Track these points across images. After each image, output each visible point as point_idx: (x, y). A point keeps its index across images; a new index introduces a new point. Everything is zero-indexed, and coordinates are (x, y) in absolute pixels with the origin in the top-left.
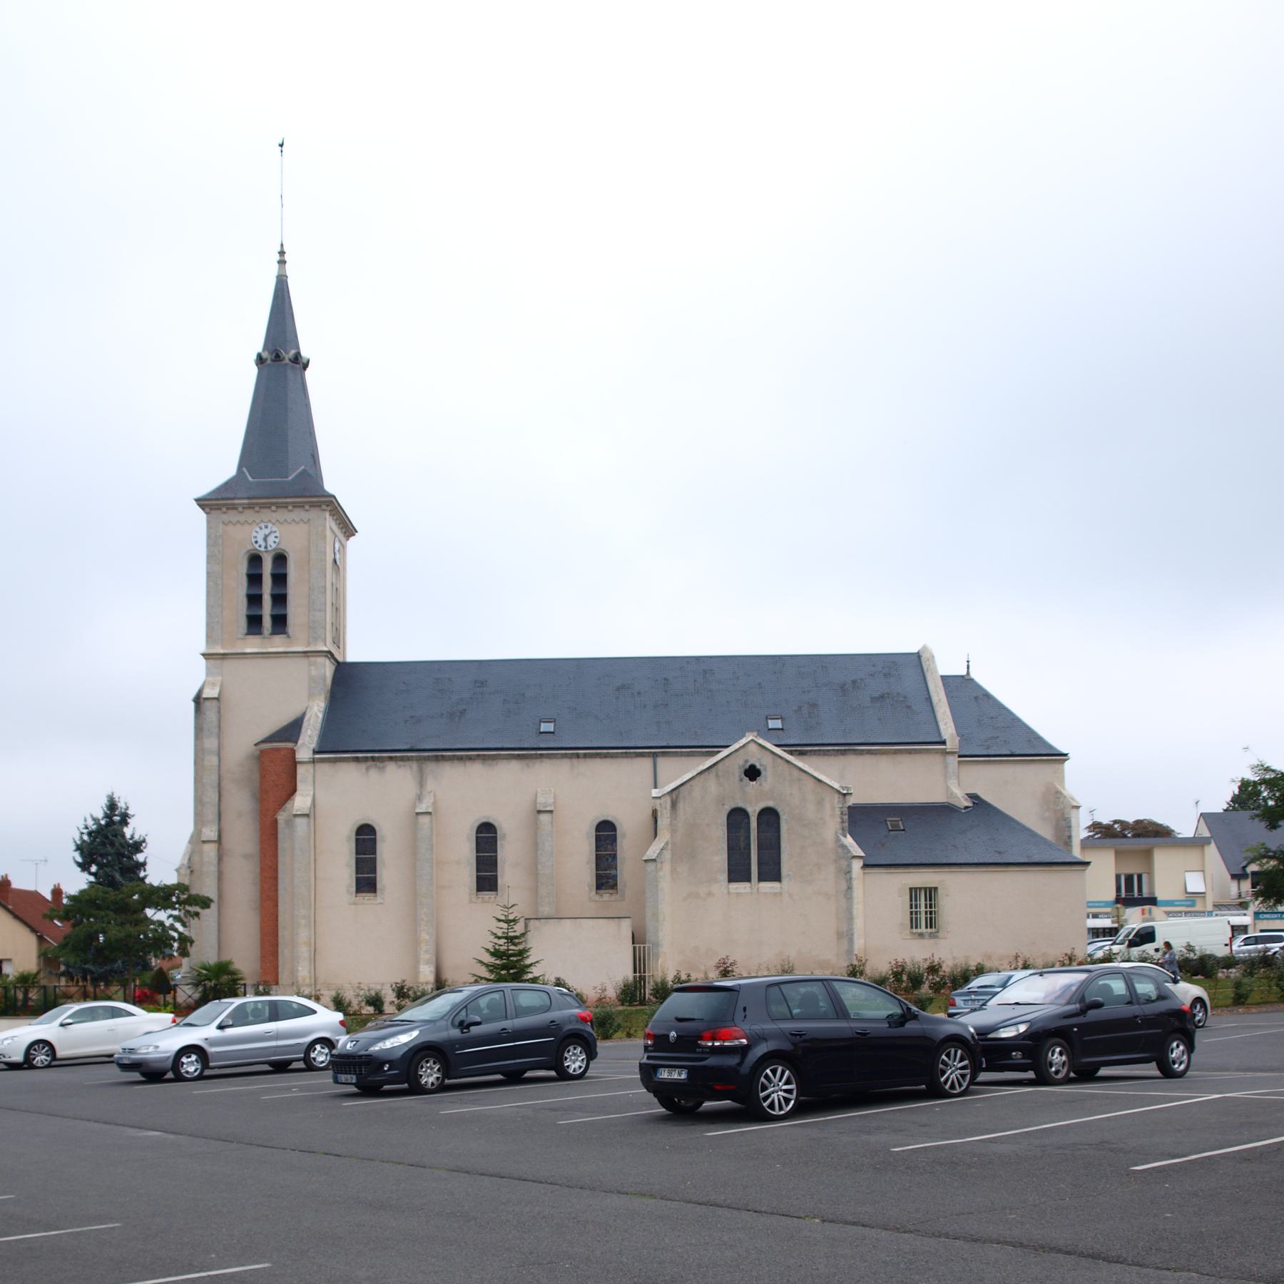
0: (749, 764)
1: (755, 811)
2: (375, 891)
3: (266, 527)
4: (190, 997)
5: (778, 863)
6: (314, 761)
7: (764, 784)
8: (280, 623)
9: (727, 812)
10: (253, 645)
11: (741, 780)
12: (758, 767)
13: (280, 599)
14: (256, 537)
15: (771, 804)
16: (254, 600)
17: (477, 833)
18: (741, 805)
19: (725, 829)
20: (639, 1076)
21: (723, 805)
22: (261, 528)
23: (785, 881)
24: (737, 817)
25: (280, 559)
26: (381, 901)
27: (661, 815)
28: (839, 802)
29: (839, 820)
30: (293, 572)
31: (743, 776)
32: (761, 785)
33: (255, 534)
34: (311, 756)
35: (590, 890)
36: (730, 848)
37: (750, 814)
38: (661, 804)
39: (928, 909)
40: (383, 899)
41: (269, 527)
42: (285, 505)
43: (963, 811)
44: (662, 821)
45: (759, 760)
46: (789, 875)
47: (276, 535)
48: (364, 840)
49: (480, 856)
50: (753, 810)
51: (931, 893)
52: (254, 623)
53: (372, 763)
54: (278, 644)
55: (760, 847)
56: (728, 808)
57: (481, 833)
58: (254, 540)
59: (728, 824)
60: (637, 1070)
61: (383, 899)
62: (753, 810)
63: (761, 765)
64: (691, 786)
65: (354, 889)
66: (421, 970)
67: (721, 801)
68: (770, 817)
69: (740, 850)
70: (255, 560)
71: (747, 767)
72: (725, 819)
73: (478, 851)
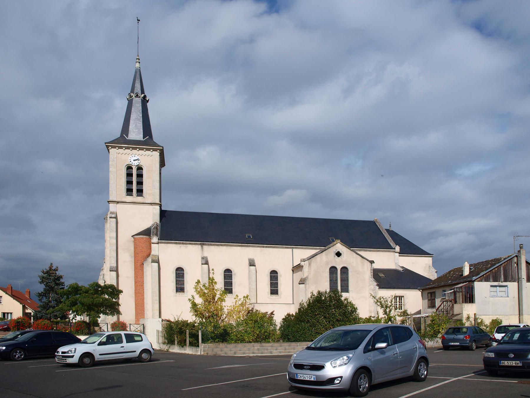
0: (337, 251)
1: (340, 267)
2: (184, 292)
3: (135, 156)
4: (137, 329)
5: (348, 286)
6: (158, 243)
7: (343, 258)
8: (140, 192)
9: (330, 267)
10: (129, 199)
11: (335, 257)
12: (341, 252)
13: (140, 183)
14: (131, 161)
15: (345, 265)
16: (129, 183)
17: (224, 273)
18: (334, 265)
19: (329, 273)
20: (483, 366)
21: (328, 265)
22: (132, 156)
23: (350, 293)
24: (333, 270)
25: (140, 168)
26: (186, 296)
27: (305, 268)
28: (370, 266)
29: (370, 272)
30: (145, 173)
31: (335, 255)
32: (342, 259)
33: (130, 159)
34: (157, 241)
35: (268, 295)
36: (330, 280)
37: (338, 269)
38: (305, 264)
39: (395, 303)
40: (187, 295)
41: (136, 156)
42: (136, 148)
43: (402, 272)
44: (305, 270)
45: (341, 250)
46: (352, 291)
47: (138, 161)
48: (179, 273)
49: (226, 281)
50: (339, 268)
51: (401, 297)
52: (129, 191)
53: (182, 245)
54: (139, 199)
55: (341, 280)
56: (330, 266)
57: (226, 273)
58: (129, 161)
59: (330, 272)
60: (482, 362)
61: (187, 295)
62: (339, 268)
63: (342, 252)
64: (316, 258)
65: (175, 291)
66: (467, 325)
67: (327, 263)
68: (345, 270)
69: (334, 281)
70: (129, 168)
71: (337, 252)
72: (329, 270)
73: (225, 279)
